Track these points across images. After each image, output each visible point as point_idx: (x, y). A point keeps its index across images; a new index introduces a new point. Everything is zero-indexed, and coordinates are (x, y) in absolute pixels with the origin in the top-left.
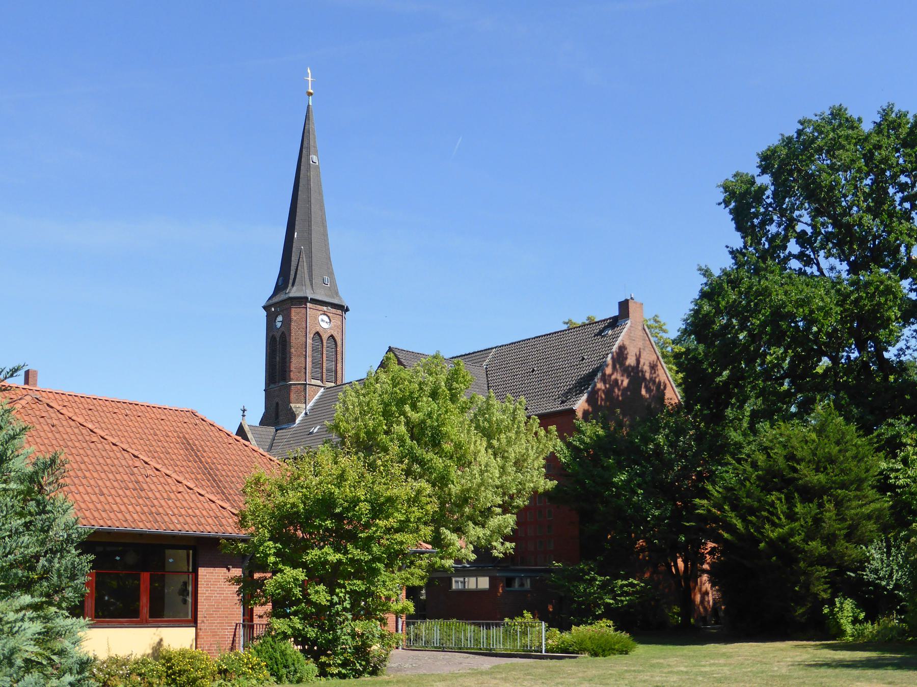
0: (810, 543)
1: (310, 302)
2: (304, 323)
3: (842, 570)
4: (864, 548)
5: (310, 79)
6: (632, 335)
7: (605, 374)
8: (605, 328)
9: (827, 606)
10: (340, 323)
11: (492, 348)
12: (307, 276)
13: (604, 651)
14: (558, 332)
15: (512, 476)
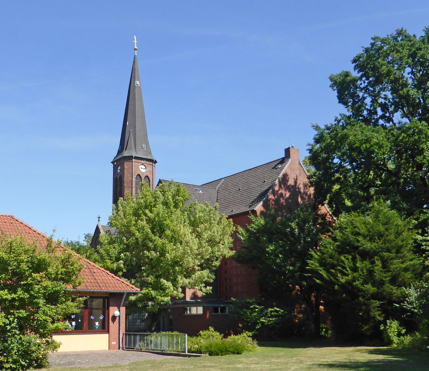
0: (365, 286)
1: (134, 159)
2: (131, 170)
3: (391, 302)
4: (404, 289)
5: (135, 41)
6: (292, 167)
7: (274, 190)
8: (278, 164)
9: (382, 325)
10: (151, 169)
11: (222, 179)
12: (133, 145)
13: (222, 352)
14: (255, 168)
15: (207, 250)
